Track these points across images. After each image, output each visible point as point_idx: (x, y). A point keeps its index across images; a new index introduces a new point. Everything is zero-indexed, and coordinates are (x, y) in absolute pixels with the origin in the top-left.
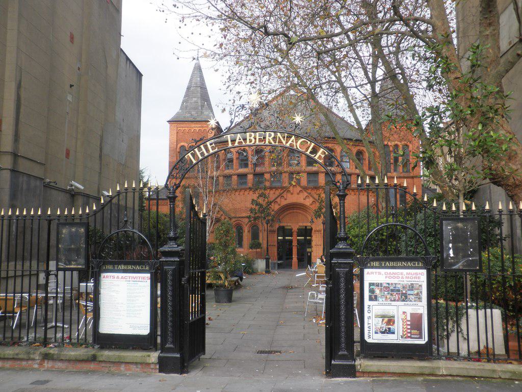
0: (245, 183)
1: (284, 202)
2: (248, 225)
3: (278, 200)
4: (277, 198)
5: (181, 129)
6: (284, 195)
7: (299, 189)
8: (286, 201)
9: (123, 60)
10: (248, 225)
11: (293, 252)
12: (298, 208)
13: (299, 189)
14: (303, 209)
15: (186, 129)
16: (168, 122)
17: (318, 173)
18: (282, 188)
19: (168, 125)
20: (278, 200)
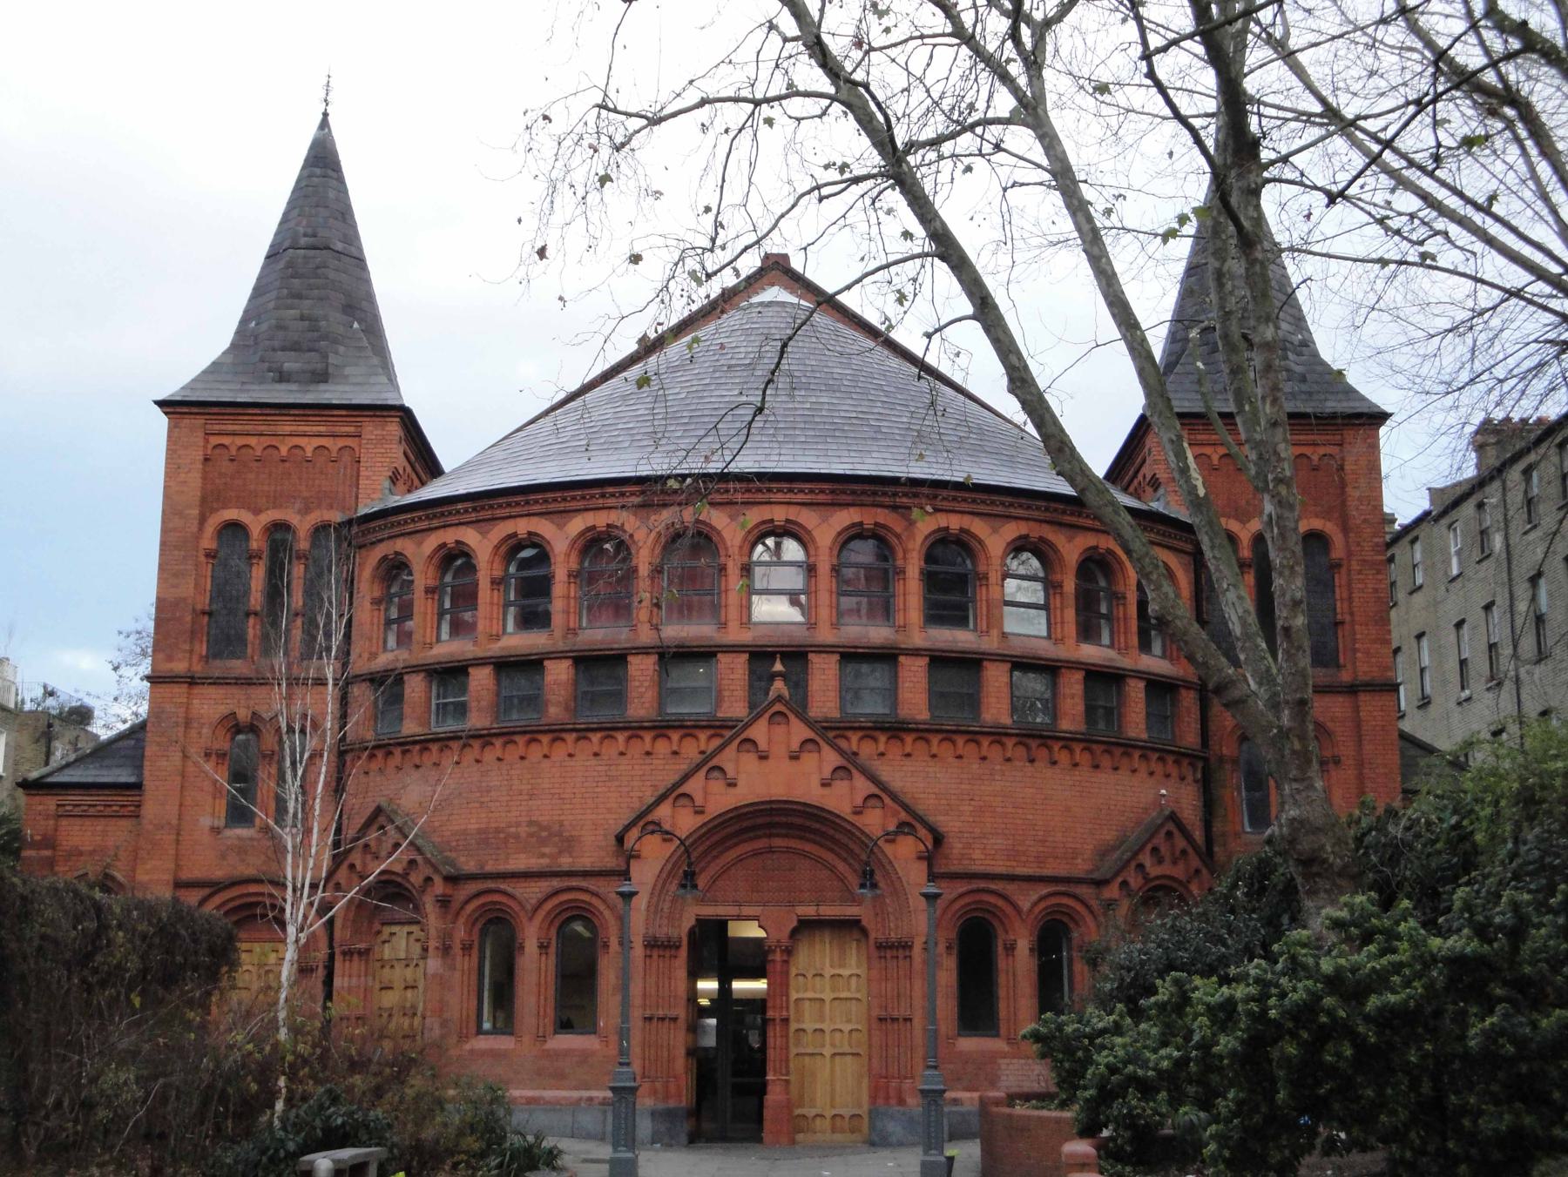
0: (534, 701)
1: (721, 800)
3: (694, 786)
4: (686, 777)
5: (226, 440)
6: (728, 759)
7: (799, 731)
8: (732, 790)
10: (541, 914)
13: (799, 731)
15: (252, 441)
16: (161, 404)
18: (717, 726)
19: (161, 421)
20: (694, 786)
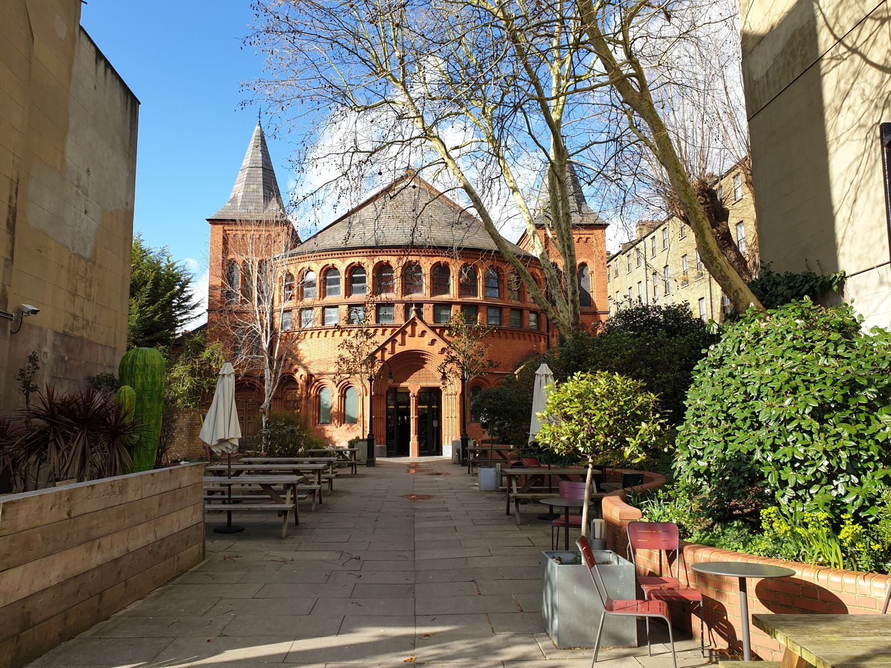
9: (86, 57)
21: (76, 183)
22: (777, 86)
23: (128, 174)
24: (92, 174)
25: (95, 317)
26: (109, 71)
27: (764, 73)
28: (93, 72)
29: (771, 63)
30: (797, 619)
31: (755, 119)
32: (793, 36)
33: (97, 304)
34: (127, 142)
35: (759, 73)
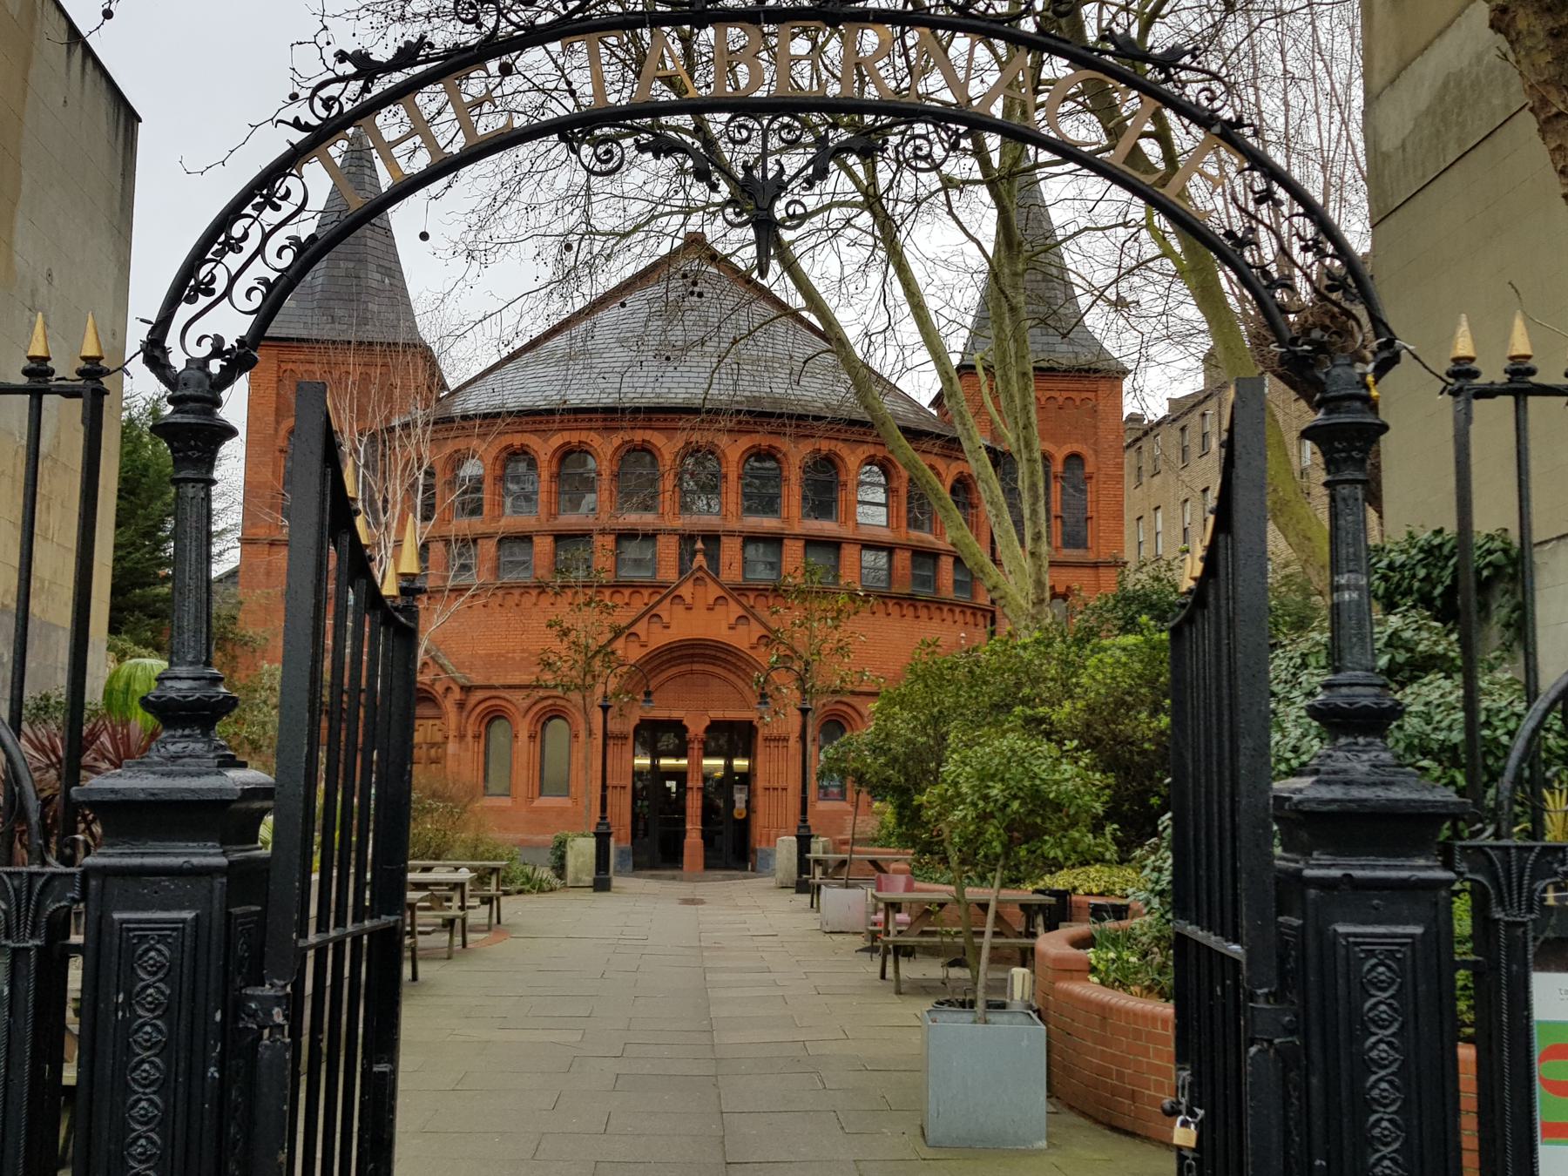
1: (659, 638)
2: (531, 714)
3: (640, 628)
7: (714, 591)
9: (53, 48)
10: (531, 714)
11: (689, 811)
12: (713, 660)
14: (725, 660)
17: (939, 554)
18: (656, 587)
20: (640, 628)
21: (28, 303)
22: (1420, 173)
23: (116, 271)
24: (56, 282)
25: (55, 573)
26: (90, 64)
27: (1398, 143)
28: (63, 70)
29: (1410, 125)
30: (323, 501)
31: (1383, 226)
32: (1445, 85)
33: (58, 545)
34: (117, 206)
35: (1389, 143)
